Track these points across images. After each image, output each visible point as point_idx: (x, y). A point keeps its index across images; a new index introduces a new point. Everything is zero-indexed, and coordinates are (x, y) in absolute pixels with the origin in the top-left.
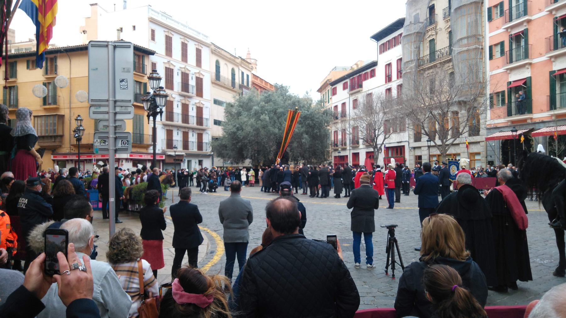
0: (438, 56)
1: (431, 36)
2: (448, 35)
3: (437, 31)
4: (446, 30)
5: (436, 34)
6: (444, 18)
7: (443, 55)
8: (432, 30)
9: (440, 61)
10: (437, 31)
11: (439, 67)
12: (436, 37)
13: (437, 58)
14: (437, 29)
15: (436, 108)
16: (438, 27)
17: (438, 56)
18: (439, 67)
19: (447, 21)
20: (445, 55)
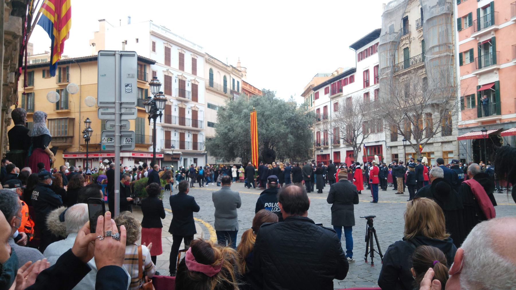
0: (412, 63)
1: (405, 45)
2: (421, 44)
3: (411, 40)
4: (419, 39)
5: (410, 42)
6: (417, 28)
7: (416, 61)
8: (406, 39)
9: (414, 68)
10: (411, 40)
11: (413, 73)
12: (410, 46)
13: (411, 64)
14: (410, 38)
15: (411, 110)
16: (412, 37)
17: (412, 63)
18: (413, 73)
19: (420, 31)
20: (418, 61)
